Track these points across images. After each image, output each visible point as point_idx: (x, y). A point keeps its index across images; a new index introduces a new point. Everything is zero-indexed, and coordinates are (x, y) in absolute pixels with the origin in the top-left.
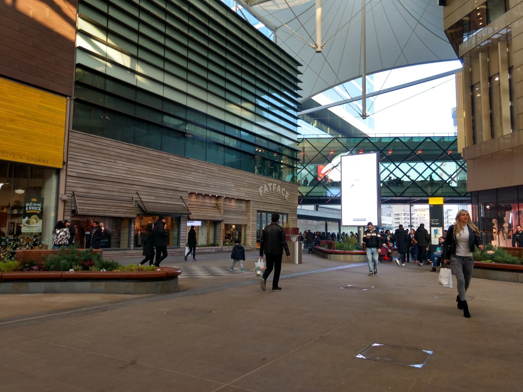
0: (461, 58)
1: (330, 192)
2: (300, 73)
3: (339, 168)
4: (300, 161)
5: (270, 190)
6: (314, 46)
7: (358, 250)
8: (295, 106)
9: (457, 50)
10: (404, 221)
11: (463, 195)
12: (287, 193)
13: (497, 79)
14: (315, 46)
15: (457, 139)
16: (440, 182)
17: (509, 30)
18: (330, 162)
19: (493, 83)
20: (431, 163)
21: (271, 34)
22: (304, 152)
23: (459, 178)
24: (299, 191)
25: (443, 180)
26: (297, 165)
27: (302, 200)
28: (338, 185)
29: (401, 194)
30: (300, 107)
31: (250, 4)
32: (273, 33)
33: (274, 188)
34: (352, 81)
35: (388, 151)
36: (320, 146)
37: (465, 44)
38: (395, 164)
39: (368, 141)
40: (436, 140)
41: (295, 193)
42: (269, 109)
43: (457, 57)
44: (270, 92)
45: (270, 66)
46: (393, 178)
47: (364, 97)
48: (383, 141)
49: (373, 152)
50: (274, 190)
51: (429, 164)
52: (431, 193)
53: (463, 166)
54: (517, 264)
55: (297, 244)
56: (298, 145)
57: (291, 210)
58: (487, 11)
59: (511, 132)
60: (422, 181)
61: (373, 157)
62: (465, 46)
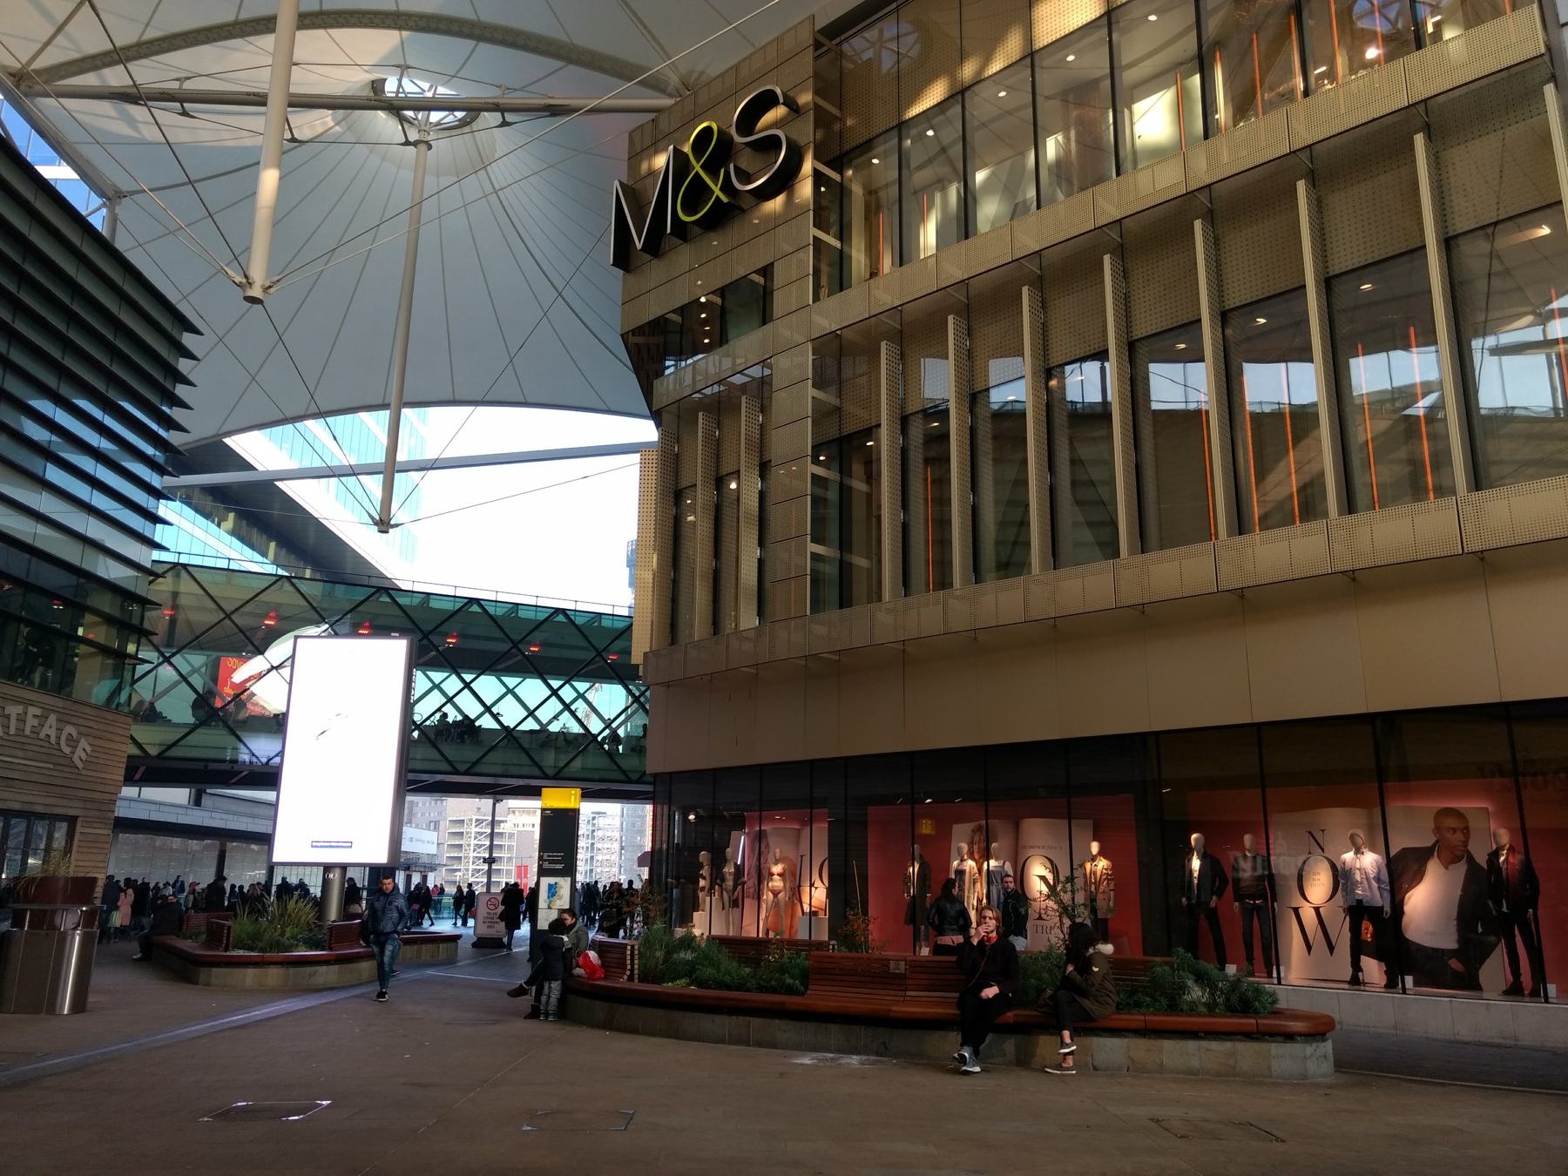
0: (657, 416)
1: (248, 748)
2: (190, 355)
3: (286, 672)
4: (155, 639)
5: (12, 731)
6: (239, 279)
7: (311, 950)
8: (157, 453)
9: (648, 393)
10: (476, 842)
11: (634, 777)
12: (83, 743)
13: (733, 486)
14: (244, 281)
15: (632, 625)
16: (580, 739)
17: (767, 372)
18: (260, 650)
19: (725, 495)
20: (563, 682)
21: (96, 206)
22: (175, 607)
23: (631, 726)
24: (132, 738)
25: (590, 732)
26: (141, 648)
27: (142, 769)
28: (277, 724)
29: (469, 768)
30: (178, 461)
31: (30, 87)
32: (104, 205)
33: (31, 722)
34: (363, 415)
35: (448, 635)
36: (231, 596)
37: (668, 380)
38: (462, 675)
39: (388, 600)
40: (579, 621)
41: (115, 746)
42: (53, 448)
43: (647, 412)
44: (65, 390)
45: (76, 308)
46: (453, 716)
47: (390, 468)
48: (434, 604)
49: (398, 635)
50: (27, 732)
51: (555, 684)
52: (555, 767)
53: (642, 699)
54: (748, 990)
55: (77, 938)
56: (150, 582)
57: (88, 805)
58: (723, 311)
59: (757, 623)
60: (532, 732)
61: (396, 649)
62: (668, 386)
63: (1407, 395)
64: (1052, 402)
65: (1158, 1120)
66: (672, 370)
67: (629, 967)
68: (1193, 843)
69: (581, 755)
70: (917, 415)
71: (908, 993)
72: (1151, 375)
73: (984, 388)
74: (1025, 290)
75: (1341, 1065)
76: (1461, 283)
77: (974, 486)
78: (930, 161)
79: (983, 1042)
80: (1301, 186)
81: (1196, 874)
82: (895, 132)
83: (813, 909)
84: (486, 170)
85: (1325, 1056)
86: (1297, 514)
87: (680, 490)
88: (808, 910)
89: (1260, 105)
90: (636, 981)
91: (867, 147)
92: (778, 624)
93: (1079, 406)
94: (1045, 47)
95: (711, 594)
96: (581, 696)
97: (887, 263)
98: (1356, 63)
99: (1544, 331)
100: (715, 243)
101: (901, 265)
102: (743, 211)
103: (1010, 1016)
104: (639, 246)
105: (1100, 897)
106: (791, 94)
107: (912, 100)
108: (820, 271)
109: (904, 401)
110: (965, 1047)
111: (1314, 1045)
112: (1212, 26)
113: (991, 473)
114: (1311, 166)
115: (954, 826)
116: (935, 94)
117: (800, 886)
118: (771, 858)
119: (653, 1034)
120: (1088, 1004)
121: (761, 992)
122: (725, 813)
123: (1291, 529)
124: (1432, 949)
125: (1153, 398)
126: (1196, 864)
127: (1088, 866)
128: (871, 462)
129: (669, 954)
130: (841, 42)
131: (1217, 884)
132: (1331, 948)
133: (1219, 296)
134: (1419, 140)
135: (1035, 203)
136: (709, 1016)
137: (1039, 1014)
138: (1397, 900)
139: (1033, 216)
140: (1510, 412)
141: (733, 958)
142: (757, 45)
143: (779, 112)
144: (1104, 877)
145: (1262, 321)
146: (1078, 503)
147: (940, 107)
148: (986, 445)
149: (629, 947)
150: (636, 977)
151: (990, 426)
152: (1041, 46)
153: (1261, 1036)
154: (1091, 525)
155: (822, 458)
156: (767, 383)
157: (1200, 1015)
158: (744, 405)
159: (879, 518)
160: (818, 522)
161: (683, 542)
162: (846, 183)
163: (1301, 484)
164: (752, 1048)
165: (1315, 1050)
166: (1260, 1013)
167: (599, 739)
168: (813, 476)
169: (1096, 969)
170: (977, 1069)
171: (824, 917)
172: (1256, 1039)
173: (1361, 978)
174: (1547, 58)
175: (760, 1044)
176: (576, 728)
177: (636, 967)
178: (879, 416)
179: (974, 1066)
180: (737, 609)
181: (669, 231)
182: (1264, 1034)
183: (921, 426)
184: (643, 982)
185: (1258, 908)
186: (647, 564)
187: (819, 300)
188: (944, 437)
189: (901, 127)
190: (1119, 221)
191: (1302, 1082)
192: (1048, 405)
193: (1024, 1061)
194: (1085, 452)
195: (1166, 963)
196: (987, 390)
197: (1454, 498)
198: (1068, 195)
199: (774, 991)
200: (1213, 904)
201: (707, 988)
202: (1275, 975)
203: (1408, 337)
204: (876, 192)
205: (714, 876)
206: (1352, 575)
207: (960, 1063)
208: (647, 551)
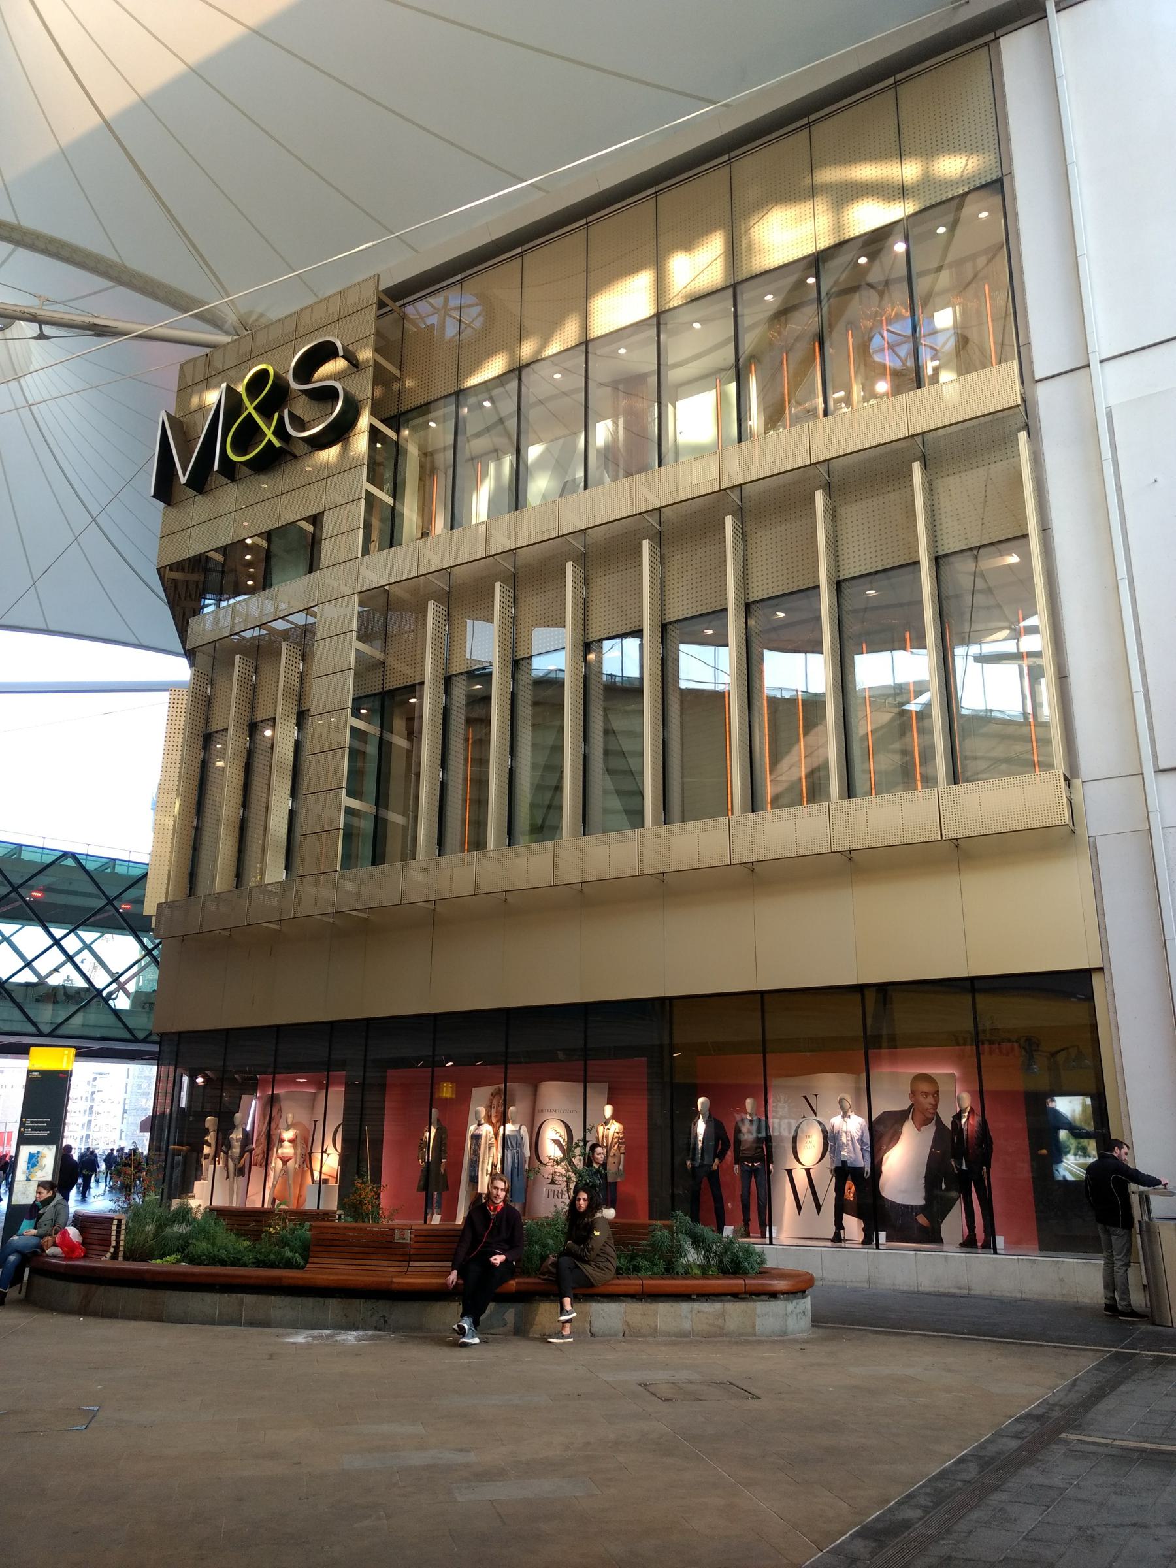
0: (190, 655)
9: (182, 630)
11: (141, 1035)
17: (311, 620)
23: (144, 980)
40: (90, 866)
51: (58, 933)
54: (245, 1265)
59: (284, 878)
60: (28, 985)
63: (900, 693)
64: (589, 675)
65: (646, 1385)
66: (211, 608)
67: (114, 1244)
68: (699, 1107)
69: (82, 1010)
70: (267, 722)
71: (412, 1263)
72: (680, 653)
73: (527, 655)
74: (569, 565)
75: (818, 1320)
76: (947, 597)
77: (512, 751)
78: (488, 429)
79: (484, 1312)
80: (819, 495)
81: (701, 1138)
82: (453, 399)
83: (323, 1177)
84: (19, 382)
85: (804, 1312)
86: (805, 795)
87: (256, 723)
88: (318, 1179)
89: (787, 418)
90: (121, 1259)
91: (424, 409)
92: (305, 880)
93: (618, 679)
94: (598, 338)
95: (237, 844)
96: (87, 947)
97: (439, 524)
98: (870, 395)
99: (1017, 644)
100: (265, 486)
101: (452, 528)
102: (295, 457)
103: (512, 1284)
104: (183, 480)
105: (611, 1160)
106: (351, 348)
107: (472, 371)
108: (371, 525)
109: (447, 665)
110: (465, 1318)
111: (795, 1302)
112: (749, 341)
113: (529, 738)
114: (740, 504)
115: (474, 1090)
116: (495, 367)
117: (311, 1153)
118: (282, 1124)
119: (135, 1318)
120: (588, 1269)
121: (258, 1267)
122: (236, 1076)
123: (797, 809)
124: (904, 1205)
125: (681, 676)
126: (701, 1127)
127: (601, 1129)
128: (413, 718)
129: (160, 1227)
130: (404, 305)
131: (720, 1147)
132: (818, 1207)
133: (744, 589)
134: (916, 467)
135: (583, 484)
136: (199, 1295)
137: (542, 1281)
138: (876, 1161)
139: (581, 496)
140: (989, 714)
141: (232, 1230)
142: (321, 297)
143: (337, 365)
144: (615, 1141)
145: (781, 615)
146: (609, 771)
147: (500, 380)
148: (526, 711)
149: (115, 1222)
150: (121, 1254)
151: (530, 692)
152: (596, 336)
153: (748, 1296)
154: (620, 793)
155: (363, 711)
156: (310, 631)
157: (694, 1277)
158: (284, 651)
159: (418, 775)
160: (355, 774)
161: (209, 788)
162: (401, 442)
163: (809, 770)
164: (243, 1328)
165: (795, 1308)
166: (749, 1273)
167: (104, 994)
168: (353, 729)
169: (597, 1234)
170: (476, 1340)
171: (334, 1184)
172: (743, 1299)
173: (842, 1236)
174: (1022, 409)
175: (252, 1324)
176: (80, 983)
177: (122, 1243)
178: (423, 674)
179: (473, 1337)
180: (263, 861)
181: (216, 468)
182: (751, 1294)
183: (464, 688)
184: (128, 1260)
185: (755, 1170)
186: (169, 809)
187: (368, 554)
188: (486, 699)
189: (459, 395)
190: (659, 509)
191: (782, 1338)
192: (513, 694)
193: (521, 1331)
194: (618, 724)
195: (666, 1227)
196: (530, 658)
197: (936, 789)
198: (615, 478)
199: (272, 1265)
200: (715, 1167)
201: (199, 1264)
202: (768, 1235)
203: (904, 640)
204: (432, 454)
205: (220, 1142)
206: (848, 855)
207: (459, 1334)
208: (170, 796)
